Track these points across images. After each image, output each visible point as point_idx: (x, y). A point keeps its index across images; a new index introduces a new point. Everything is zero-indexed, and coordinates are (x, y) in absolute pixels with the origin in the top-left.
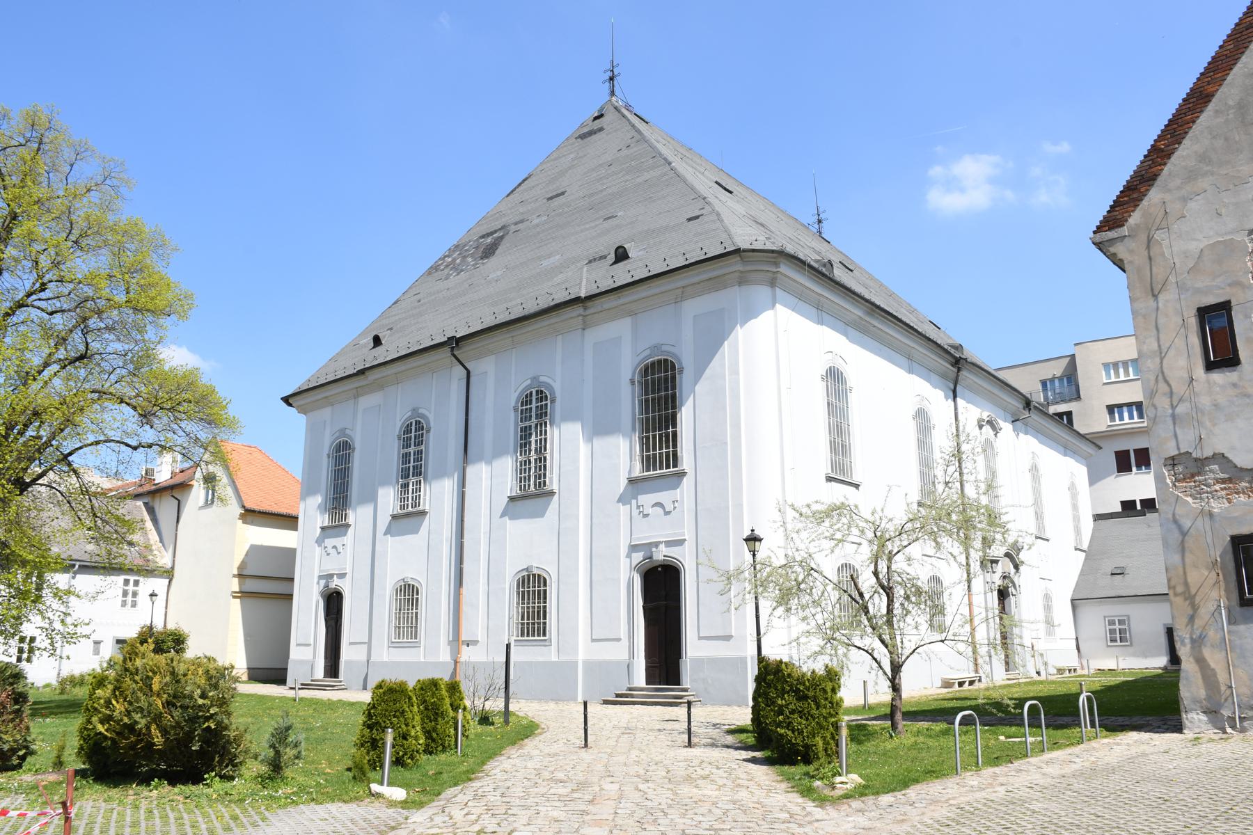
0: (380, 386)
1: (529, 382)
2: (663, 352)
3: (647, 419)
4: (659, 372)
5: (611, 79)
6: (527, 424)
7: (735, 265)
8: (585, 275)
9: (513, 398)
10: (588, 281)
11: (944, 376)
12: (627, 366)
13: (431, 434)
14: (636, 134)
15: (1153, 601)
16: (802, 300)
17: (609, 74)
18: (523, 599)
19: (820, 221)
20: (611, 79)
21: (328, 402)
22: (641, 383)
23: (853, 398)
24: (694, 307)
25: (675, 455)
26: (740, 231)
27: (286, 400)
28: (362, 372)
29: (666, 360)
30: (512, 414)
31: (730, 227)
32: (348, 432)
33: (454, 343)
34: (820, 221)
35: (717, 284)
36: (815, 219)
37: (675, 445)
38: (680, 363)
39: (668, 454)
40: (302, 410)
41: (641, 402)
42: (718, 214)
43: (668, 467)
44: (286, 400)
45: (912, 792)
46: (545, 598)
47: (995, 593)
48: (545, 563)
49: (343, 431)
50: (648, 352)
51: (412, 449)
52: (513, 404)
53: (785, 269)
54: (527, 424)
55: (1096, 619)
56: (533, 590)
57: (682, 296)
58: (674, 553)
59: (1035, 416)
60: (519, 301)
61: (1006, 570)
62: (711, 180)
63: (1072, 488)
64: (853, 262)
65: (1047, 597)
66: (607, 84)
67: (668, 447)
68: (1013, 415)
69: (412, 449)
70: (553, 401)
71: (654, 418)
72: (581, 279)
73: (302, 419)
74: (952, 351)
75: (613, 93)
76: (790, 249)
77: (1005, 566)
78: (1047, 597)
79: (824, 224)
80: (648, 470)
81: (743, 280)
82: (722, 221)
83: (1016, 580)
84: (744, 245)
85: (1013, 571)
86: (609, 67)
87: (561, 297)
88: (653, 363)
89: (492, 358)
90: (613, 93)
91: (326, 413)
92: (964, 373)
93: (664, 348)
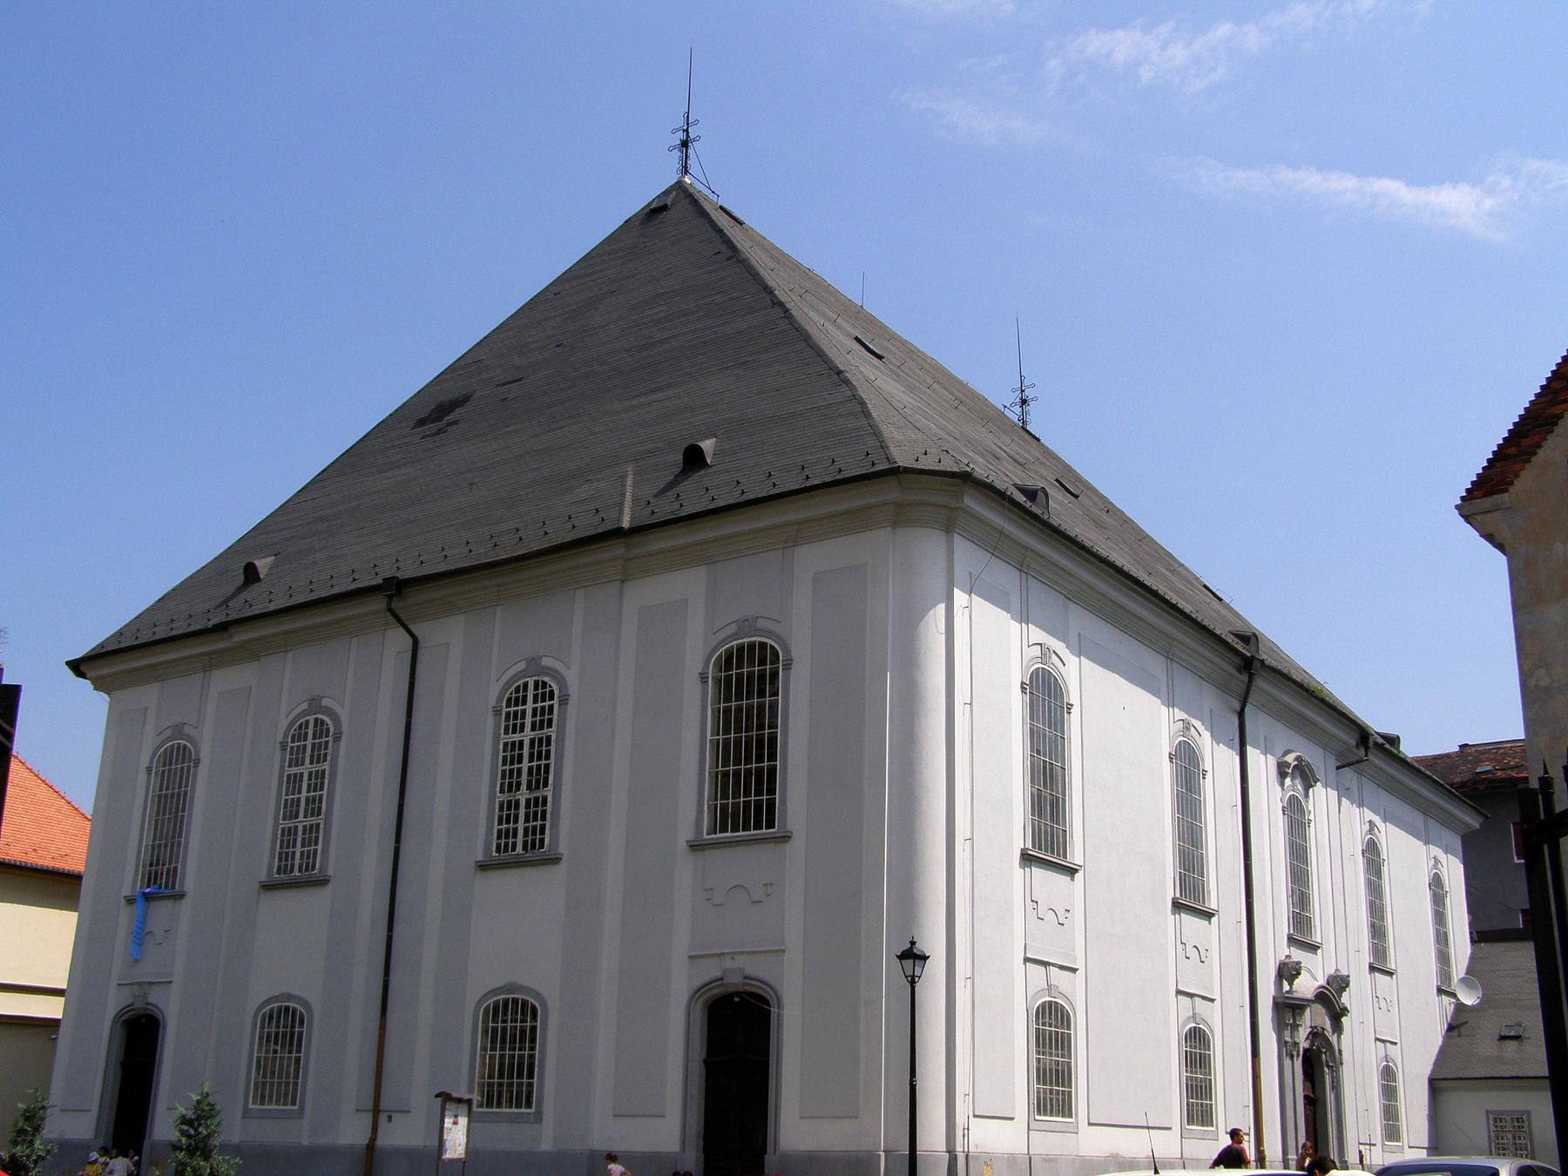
0: (250, 653)
1: (522, 666)
2: (759, 631)
3: (726, 743)
4: (751, 663)
5: (685, 144)
6: (517, 737)
7: (888, 492)
8: (629, 490)
9: (493, 692)
10: (635, 500)
11: (1223, 687)
12: (696, 650)
13: (343, 744)
14: (723, 248)
15: (1521, 1089)
16: (996, 545)
17: (681, 135)
18: (494, 1041)
19: (1024, 402)
20: (685, 144)
21: (152, 674)
22: (717, 681)
23: (1074, 721)
24: (813, 558)
25: (771, 805)
26: (898, 435)
27: (77, 667)
28: (223, 628)
29: (763, 645)
30: (491, 720)
31: (883, 427)
32: (187, 729)
33: (394, 593)
34: (1024, 402)
35: (856, 521)
36: (1016, 397)
37: (772, 791)
38: (787, 650)
39: (759, 805)
40: (100, 685)
41: (716, 712)
42: (862, 403)
43: (758, 826)
44: (77, 667)
45: (771, 283)
46: (533, 1040)
47: (1298, 1063)
48: (542, 978)
49: (178, 730)
50: (732, 629)
51: (306, 768)
52: (492, 701)
53: (972, 503)
54: (517, 737)
55: (1472, 1110)
56: (513, 1028)
57: (798, 534)
58: (759, 969)
59: (1375, 758)
60: (513, 525)
61: (1318, 1023)
62: (848, 335)
63: (1436, 883)
64: (1079, 479)
65: (1388, 1073)
66: (677, 154)
67: (759, 792)
68: (1339, 756)
69: (306, 768)
70: (564, 701)
71: (738, 742)
72: (623, 495)
73: (101, 701)
74: (1240, 646)
75: (685, 170)
76: (980, 472)
77: (1314, 1017)
78: (1388, 1073)
79: (1031, 407)
80: (724, 829)
81: (900, 517)
82: (868, 415)
83: (1334, 1039)
84: (902, 462)
85: (1328, 1024)
86: (681, 123)
87: (587, 526)
88: (741, 648)
89: (462, 617)
90: (685, 170)
91: (149, 695)
92: (1260, 682)
93: (761, 624)
